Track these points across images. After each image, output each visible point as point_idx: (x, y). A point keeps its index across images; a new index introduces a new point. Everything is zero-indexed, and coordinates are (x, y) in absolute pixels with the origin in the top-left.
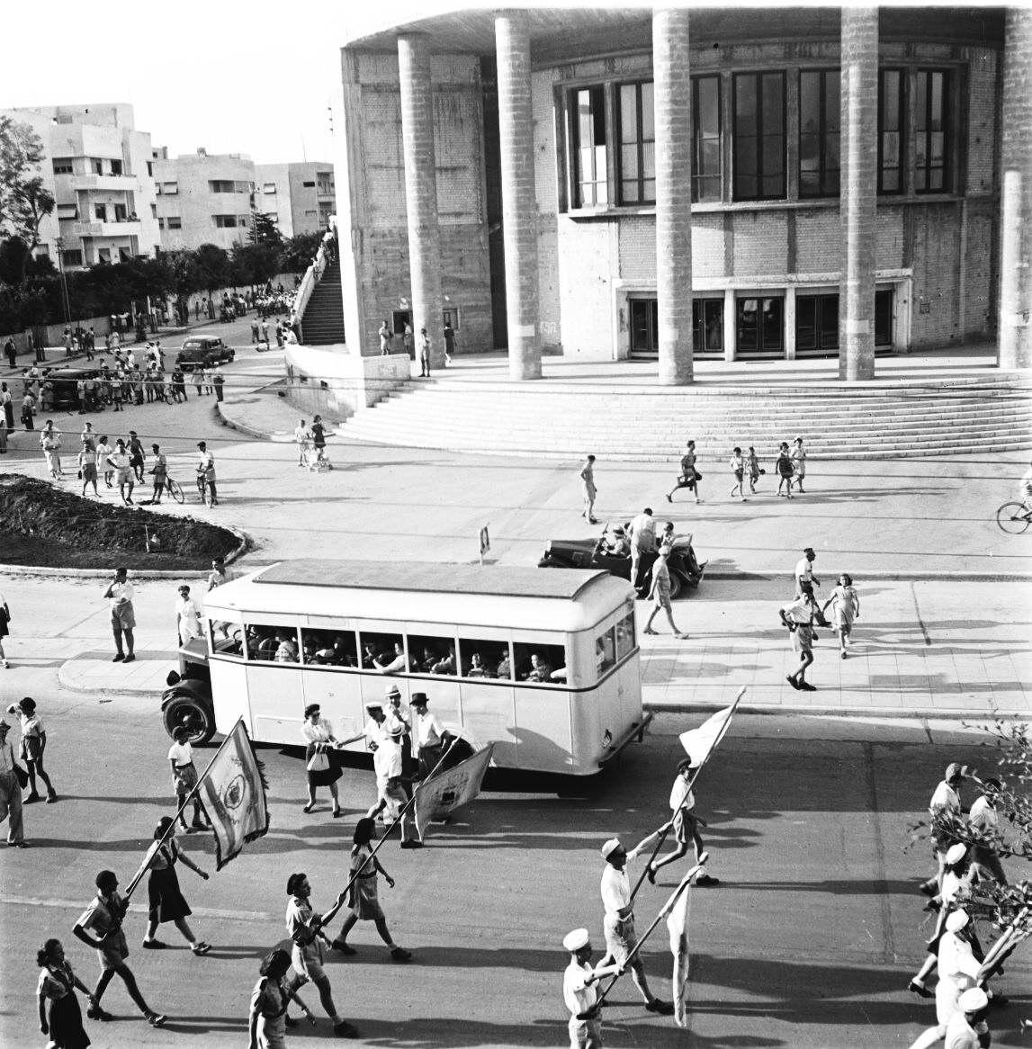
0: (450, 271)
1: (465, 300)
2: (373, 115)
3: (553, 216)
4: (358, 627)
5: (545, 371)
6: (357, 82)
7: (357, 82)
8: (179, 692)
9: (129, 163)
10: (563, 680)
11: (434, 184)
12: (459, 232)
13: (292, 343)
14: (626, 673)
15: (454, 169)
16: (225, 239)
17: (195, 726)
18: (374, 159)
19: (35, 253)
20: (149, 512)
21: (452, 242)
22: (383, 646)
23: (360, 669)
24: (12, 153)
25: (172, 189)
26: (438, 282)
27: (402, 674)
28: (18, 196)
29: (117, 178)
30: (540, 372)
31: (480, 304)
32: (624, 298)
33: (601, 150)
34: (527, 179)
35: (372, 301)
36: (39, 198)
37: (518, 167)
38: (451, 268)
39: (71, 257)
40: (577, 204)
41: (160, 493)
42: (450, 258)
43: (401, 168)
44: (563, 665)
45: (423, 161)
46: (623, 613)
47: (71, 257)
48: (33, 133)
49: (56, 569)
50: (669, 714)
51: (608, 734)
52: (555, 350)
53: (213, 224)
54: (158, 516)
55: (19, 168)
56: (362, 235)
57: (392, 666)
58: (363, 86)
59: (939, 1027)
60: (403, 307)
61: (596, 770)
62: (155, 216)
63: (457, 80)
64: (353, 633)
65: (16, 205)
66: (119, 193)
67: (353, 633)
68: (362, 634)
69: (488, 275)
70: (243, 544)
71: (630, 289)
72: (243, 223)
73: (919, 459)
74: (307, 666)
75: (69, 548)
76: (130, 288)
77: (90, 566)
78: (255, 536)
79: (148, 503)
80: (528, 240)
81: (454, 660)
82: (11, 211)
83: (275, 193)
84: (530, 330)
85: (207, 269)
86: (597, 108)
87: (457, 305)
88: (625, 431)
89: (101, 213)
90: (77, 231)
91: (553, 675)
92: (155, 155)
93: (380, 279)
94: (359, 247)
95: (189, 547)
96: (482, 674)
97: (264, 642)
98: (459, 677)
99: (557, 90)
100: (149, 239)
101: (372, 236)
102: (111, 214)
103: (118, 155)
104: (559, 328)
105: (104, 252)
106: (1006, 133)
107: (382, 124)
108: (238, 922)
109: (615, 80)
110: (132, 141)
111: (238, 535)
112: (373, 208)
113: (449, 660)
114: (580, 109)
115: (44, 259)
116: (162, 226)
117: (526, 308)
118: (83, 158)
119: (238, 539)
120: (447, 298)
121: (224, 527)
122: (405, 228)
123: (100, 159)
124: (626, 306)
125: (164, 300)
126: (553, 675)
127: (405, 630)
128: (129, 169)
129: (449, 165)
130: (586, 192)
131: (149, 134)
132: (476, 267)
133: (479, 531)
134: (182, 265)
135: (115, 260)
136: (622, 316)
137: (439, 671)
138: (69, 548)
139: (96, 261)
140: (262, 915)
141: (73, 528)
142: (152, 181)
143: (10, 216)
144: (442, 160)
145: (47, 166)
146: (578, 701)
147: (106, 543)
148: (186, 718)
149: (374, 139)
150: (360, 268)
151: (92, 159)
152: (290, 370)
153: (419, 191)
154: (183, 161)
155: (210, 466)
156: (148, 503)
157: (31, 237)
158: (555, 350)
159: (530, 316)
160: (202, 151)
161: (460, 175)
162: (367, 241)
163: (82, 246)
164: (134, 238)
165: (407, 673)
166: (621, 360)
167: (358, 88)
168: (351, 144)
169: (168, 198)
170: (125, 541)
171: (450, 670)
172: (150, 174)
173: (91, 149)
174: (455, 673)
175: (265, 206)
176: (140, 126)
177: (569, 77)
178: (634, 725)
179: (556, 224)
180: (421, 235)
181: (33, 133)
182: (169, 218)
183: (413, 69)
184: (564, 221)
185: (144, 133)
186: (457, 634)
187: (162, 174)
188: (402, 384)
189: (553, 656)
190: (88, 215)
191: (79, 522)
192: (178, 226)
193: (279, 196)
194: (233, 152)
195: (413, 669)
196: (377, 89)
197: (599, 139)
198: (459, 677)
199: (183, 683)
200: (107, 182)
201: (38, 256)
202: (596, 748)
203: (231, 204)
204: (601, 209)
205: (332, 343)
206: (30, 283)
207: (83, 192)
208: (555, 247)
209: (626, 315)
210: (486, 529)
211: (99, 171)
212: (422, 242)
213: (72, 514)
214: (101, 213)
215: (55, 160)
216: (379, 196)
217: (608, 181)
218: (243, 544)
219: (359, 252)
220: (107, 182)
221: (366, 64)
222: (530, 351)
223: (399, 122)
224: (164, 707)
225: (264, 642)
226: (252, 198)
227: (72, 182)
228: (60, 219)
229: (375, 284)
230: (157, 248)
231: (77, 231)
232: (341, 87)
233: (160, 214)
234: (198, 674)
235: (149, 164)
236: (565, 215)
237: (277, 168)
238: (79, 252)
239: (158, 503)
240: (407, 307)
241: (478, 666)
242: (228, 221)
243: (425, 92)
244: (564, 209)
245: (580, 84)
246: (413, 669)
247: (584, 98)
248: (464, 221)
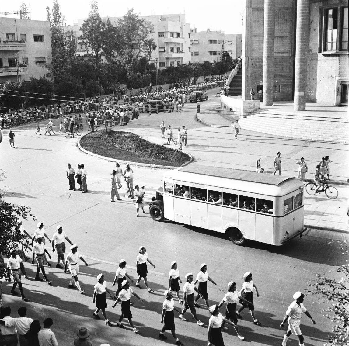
0: (278, 72)
1: (283, 82)
3: (316, 54)
4: (208, 188)
5: (307, 108)
6: (251, 7)
7: (251, 7)
8: (155, 204)
9: (183, 34)
10: (272, 213)
11: (274, 42)
12: (283, 59)
13: (222, 95)
14: (296, 214)
15: (282, 37)
16: (212, 59)
17: (158, 215)
18: (255, 33)
19: (150, 62)
20: (165, 147)
21: (280, 62)
22: (215, 195)
23: (207, 202)
24: (145, 31)
25: (197, 42)
26: (272, 76)
27: (220, 205)
28: (146, 44)
29: (178, 39)
30: (305, 108)
31: (288, 84)
32: (339, 84)
33: (335, 31)
34: (306, 40)
35: (250, 81)
36: (153, 45)
37: (302, 36)
38: (279, 71)
39: (162, 64)
40: (325, 50)
41: (170, 141)
42: (279, 67)
43: (263, 36)
44: (272, 208)
45: (270, 34)
46: (298, 192)
47: (162, 64)
48: (151, 24)
49: (133, 163)
50: (316, 230)
51: (287, 233)
52: (314, 101)
53: (209, 54)
54: (167, 148)
55: (146, 35)
56: (248, 59)
57: (217, 202)
59: (127, 263)
60: (261, 84)
61: (280, 244)
62: (190, 52)
63: (286, 6)
64: (206, 190)
65: (145, 47)
66: (179, 43)
67: (206, 190)
68: (209, 191)
70: (191, 160)
71: (342, 81)
72: (219, 54)
73: (249, 140)
74: (240, 209)
75: (139, 156)
76: (178, 75)
77: (143, 163)
78: (196, 158)
79: (166, 144)
80: (303, 62)
81: (237, 202)
82: (144, 49)
83: (231, 44)
84: (302, 94)
85: (205, 69)
86: (335, 16)
87: (280, 84)
88: (332, 131)
89: (172, 50)
90: (164, 56)
91: (269, 211)
92: (192, 31)
93: (254, 74)
94: (247, 63)
95: (174, 159)
96: (246, 208)
97: (180, 190)
98: (238, 208)
99: (321, 9)
100: (187, 59)
102: (175, 50)
103: (179, 31)
104: (315, 93)
105: (172, 62)
107: (258, 21)
108: (154, 275)
109: (342, 6)
110: (184, 27)
111: (190, 156)
112: (253, 50)
113: (236, 202)
114: (329, 16)
115: (153, 65)
116: (192, 54)
117: (301, 86)
118: (168, 32)
119: (190, 158)
120: (277, 81)
121: (187, 154)
122: (263, 57)
123: (173, 32)
124: (340, 87)
125: (184, 79)
126: (269, 211)
127: (222, 191)
128: (182, 36)
129: (281, 36)
130: (329, 45)
131: (190, 24)
132: (288, 71)
133: (257, 161)
134: (196, 68)
135: (175, 65)
136: (338, 90)
137: (232, 205)
138: (139, 156)
139: (170, 65)
140: (163, 274)
141: (141, 150)
142: (190, 39)
143: (143, 51)
144: (277, 33)
145: (156, 35)
146: (276, 219)
147: (150, 156)
148: (156, 212)
149: (255, 27)
150: (247, 70)
151: (171, 32)
152: (221, 103)
153: (268, 44)
154: (202, 33)
155: (186, 134)
156: (166, 144)
157: (148, 58)
158: (314, 101)
159: (302, 89)
160: (208, 30)
161: (285, 39)
162: (250, 61)
163: (165, 61)
164: (182, 58)
165: (222, 205)
166: (337, 106)
167: (251, 9)
168: (247, 28)
169: (196, 45)
170: (156, 155)
171: (235, 205)
172: (189, 37)
173: (170, 29)
174: (237, 207)
175: (227, 48)
176: (187, 21)
177: (326, 5)
178: (299, 231)
179: (317, 57)
180: (267, 60)
181: (151, 24)
182: (195, 52)
183: (269, 2)
184: (320, 56)
185: (188, 24)
186: (239, 194)
187: (193, 37)
188: (256, 111)
189: (270, 204)
190: (168, 51)
191: (143, 148)
192: (198, 55)
193: (233, 45)
194: (218, 30)
195: (224, 204)
196: (258, 9)
197: (335, 27)
198: (238, 208)
199: (156, 201)
200: (175, 40)
201: (151, 64)
202: (281, 237)
203: (216, 48)
204: (334, 52)
205: (238, 95)
206: (147, 72)
207: (167, 43)
208: (316, 65)
209: (340, 89)
210: (260, 160)
211: (173, 36)
212: (268, 62)
213: (142, 146)
214: (172, 50)
215: (159, 33)
216: (255, 46)
217: (337, 42)
218: (191, 160)
219: (247, 64)
220: (175, 40)
222: (302, 101)
223: (263, 21)
224: (150, 208)
225: (180, 190)
226: (223, 46)
227: (163, 40)
228: (159, 52)
229: (252, 76)
230: (190, 62)
231: (164, 56)
232: (245, 9)
233: (192, 50)
234: (160, 197)
235: (189, 34)
236: (320, 53)
237: (233, 35)
238: (164, 63)
239: (169, 144)
241: (245, 205)
242: (214, 53)
243: (273, 10)
244: (320, 52)
245: (330, 7)
246: (224, 204)
247: (331, 12)
248: (285, 55)
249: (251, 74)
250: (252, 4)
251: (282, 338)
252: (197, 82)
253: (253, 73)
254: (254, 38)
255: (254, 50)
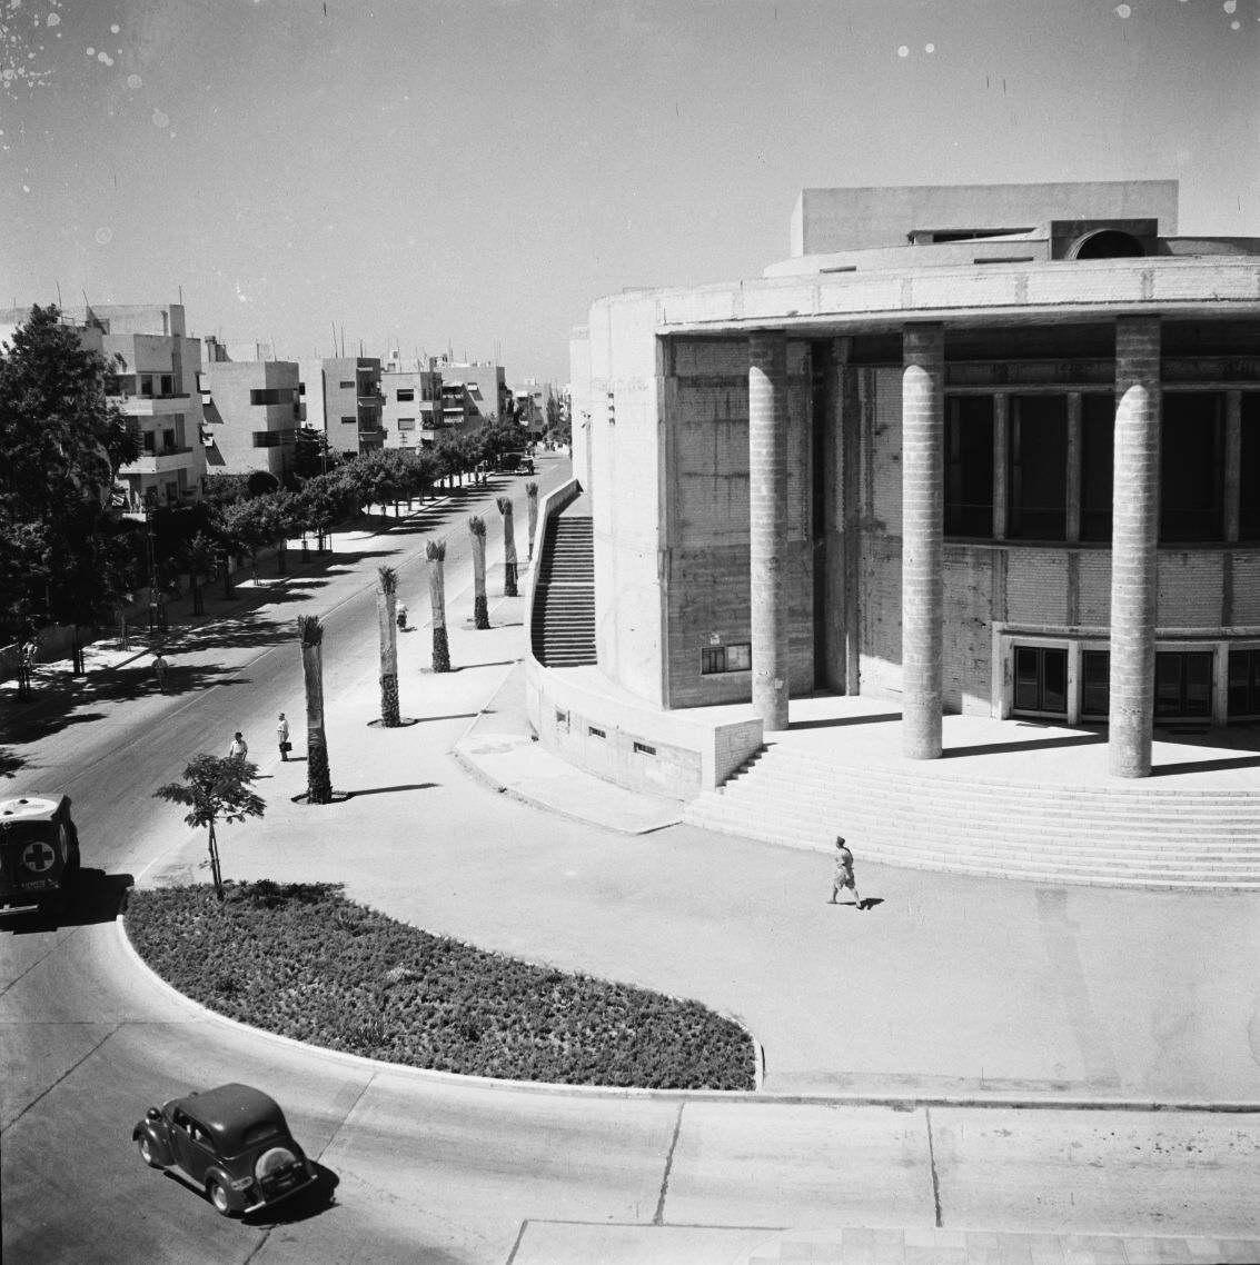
2: (690, 414)
6: (673, 375)
58: (680, 379)
69: (811, 602)
93: (689, 609)
101: (682, 557)
106: (970, 577)
107: (699, 424)
112: (684, 524)
136: (1006, 666)
167: (674, 382)
221: (684, 353)
240: (235, 747)
249: (681, 607)
250: (678, 367)
251: (1073, 527)
252: (371, 1074)
253: (687, 606)
254: (686, 483)
255: (690, 524)
